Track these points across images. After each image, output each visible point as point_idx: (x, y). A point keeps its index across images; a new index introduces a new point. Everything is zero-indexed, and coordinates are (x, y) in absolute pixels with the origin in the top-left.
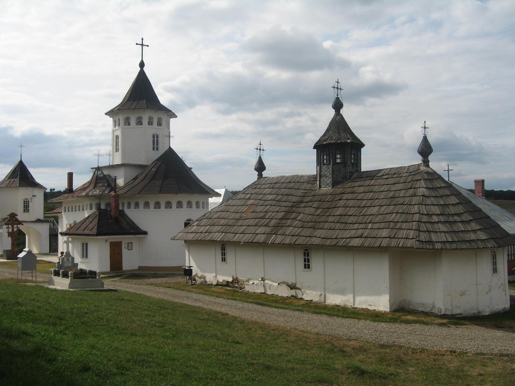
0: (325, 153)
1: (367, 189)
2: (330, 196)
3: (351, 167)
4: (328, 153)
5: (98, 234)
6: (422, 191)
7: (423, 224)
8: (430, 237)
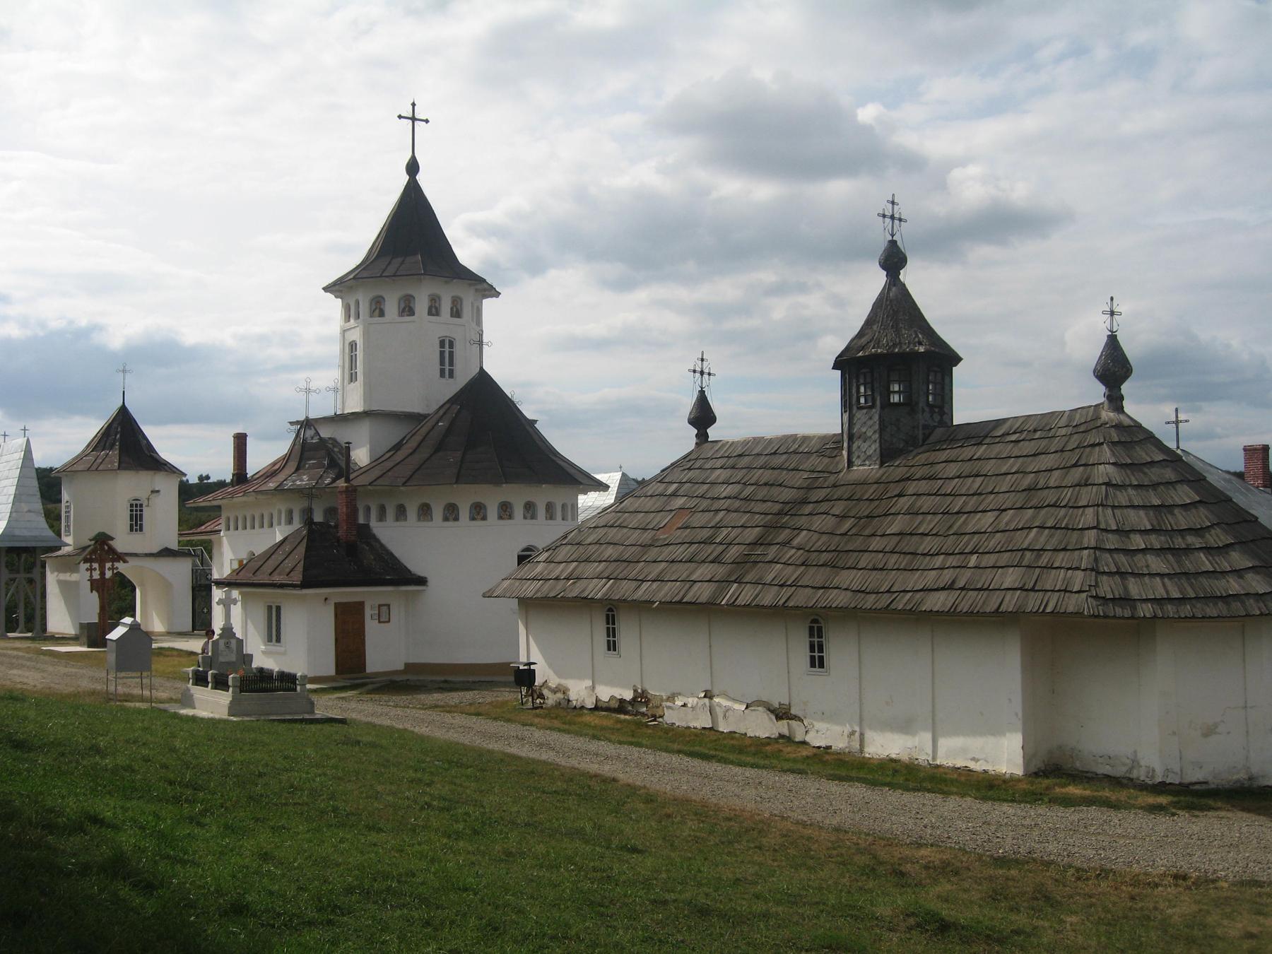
1: (967, 468)
3: (927, 415)
4: (869, 380)
5: (306, 584)
8: (1126, 589)
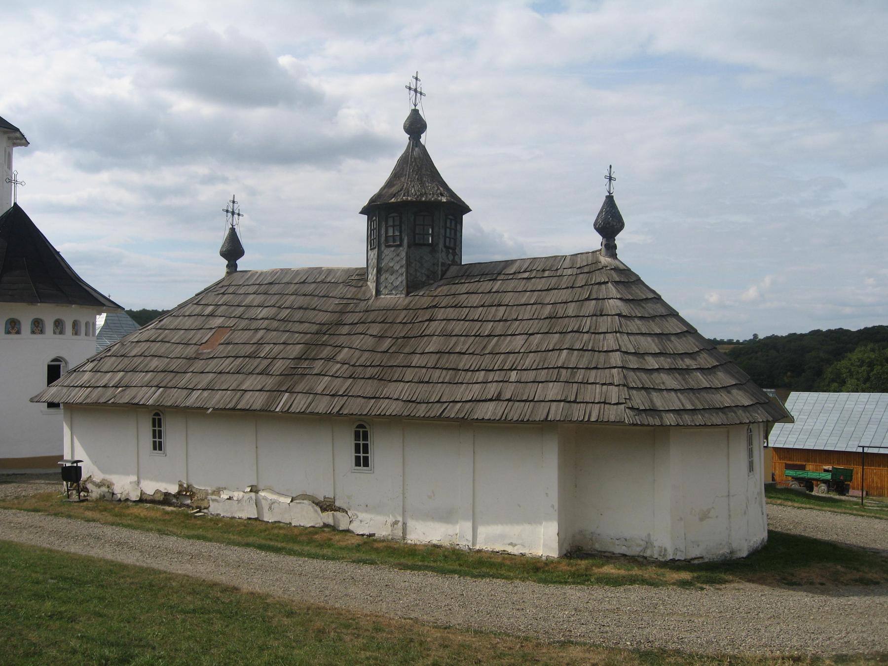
0: (390, 223)
1: (488, 299)
2: (405, 312)
3: (444, 254)
4: (397, 223)
6: (614, 305)
7: (631, 373)
8: (652, 401)
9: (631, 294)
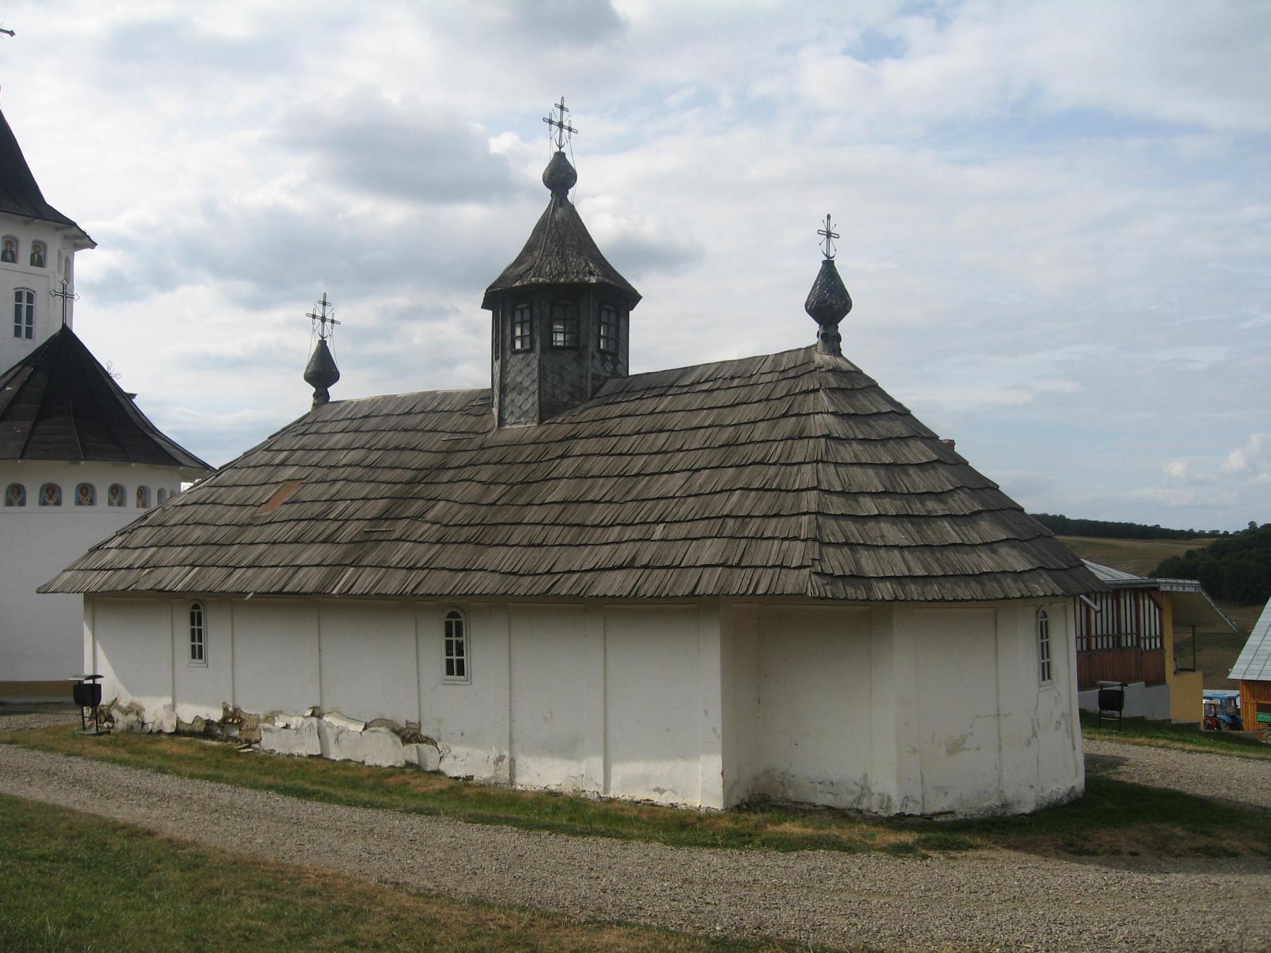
0: (518, 318)
1: (648, 422)
2: (532, 447)
3: (597, 362)
4: (527, 317)
8: (857, 563)
9: (852, 406)
